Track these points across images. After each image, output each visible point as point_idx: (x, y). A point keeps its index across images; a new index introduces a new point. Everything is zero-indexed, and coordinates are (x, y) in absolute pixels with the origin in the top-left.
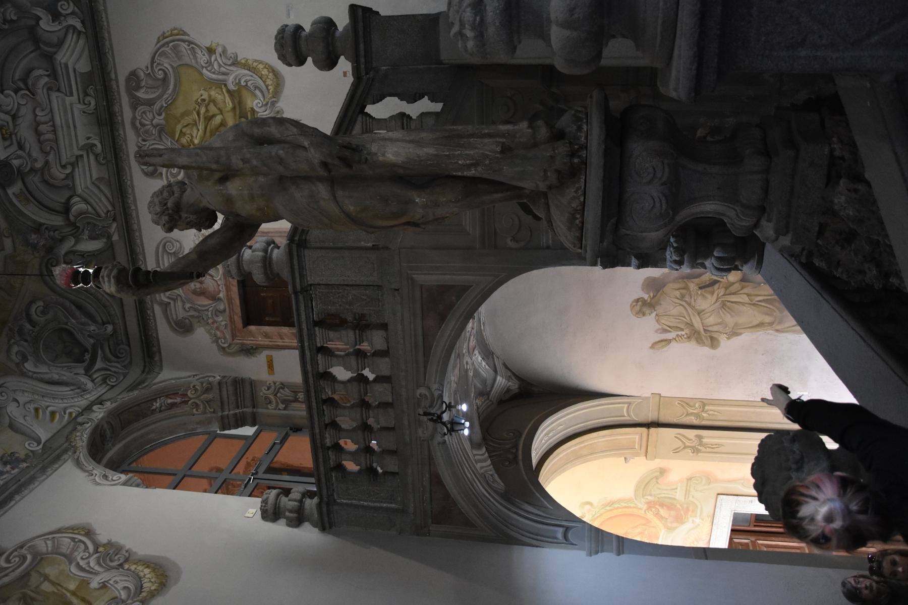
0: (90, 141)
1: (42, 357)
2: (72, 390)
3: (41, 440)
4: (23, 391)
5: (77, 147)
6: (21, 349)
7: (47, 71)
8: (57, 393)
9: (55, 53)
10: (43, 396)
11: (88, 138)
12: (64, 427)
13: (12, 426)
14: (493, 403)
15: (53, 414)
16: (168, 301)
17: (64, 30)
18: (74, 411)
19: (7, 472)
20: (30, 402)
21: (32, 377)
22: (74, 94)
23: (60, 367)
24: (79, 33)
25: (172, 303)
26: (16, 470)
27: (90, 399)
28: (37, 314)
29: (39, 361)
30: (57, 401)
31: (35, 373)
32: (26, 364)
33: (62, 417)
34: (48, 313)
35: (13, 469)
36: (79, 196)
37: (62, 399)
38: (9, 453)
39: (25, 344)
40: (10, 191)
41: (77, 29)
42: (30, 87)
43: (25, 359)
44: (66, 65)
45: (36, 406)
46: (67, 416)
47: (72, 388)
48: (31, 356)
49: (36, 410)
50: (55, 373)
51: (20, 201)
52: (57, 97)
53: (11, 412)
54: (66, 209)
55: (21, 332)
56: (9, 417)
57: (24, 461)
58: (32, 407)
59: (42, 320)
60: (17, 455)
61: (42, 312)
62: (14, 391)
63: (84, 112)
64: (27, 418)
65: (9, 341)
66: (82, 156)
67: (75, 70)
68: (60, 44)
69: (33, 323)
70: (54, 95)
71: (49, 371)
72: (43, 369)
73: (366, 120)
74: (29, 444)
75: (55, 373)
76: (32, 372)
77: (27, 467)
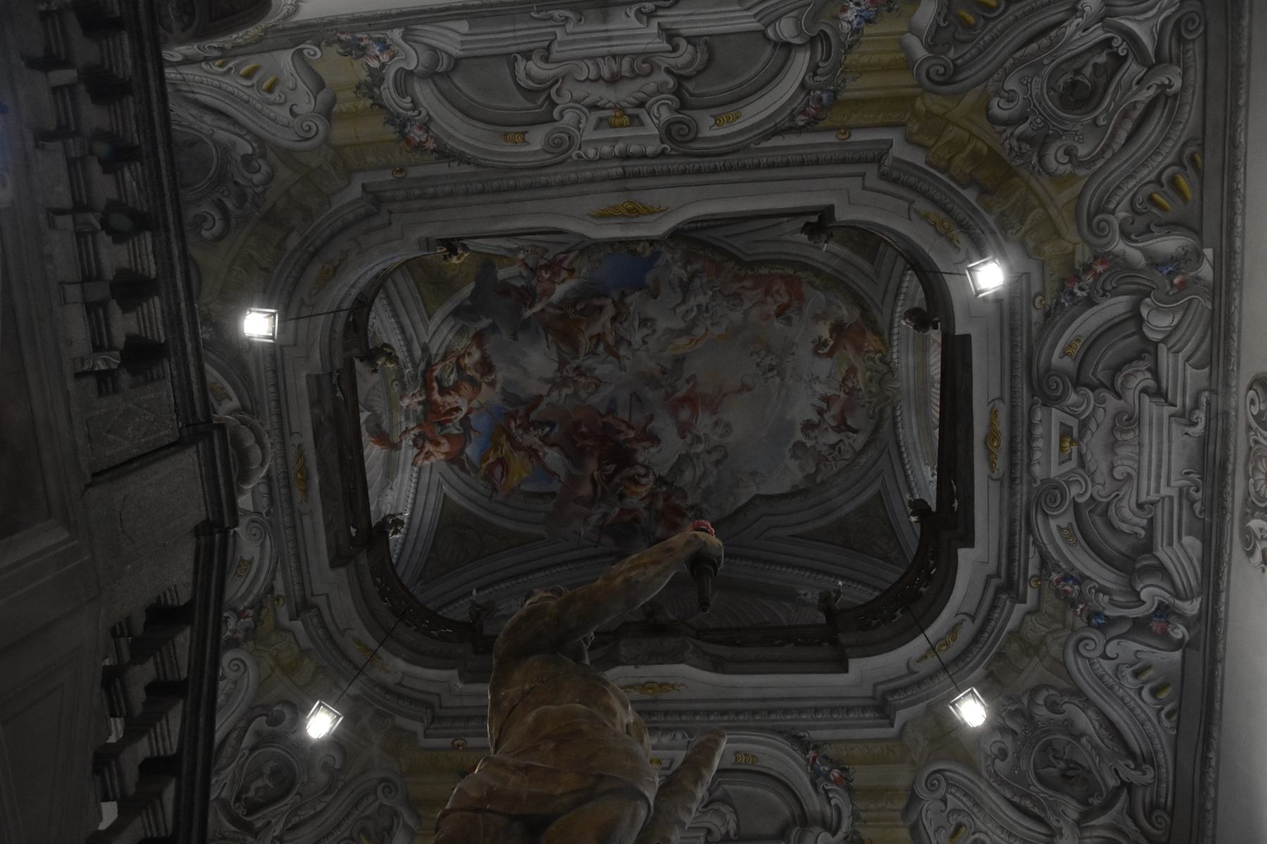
1: (217, 152)
2: (193, 92)
3: (294, 54)
4: (274, 120)
6: (246, 174)
7: (735, 835)
8: (222, 99)
10: (248, 102)
12: (242, 55)
13: (321, 85)
14: (312, 595)
15: (248, 76)
19: (371, 38)
20: (273, 104)
21: (249, 131)
23: (193, 129)
26: (359, 36)
27: (175, 71)
28: (214, 219)
29: (225, 150)
30: (230, 89)
31: (239, 135)
32: (250, 151)
33: (238, 67)
34: (195, 216)
35: (361, 39)
37: (220, 87)
38: (348, 57)
39: (239, 180)
40: (235, 403)
42: (715, 806)
43: (247, 160)
45: (269, 96)
46: (230, 65)
47: (190, 95)
48: (235, 160)
49: (270, 90)
50: (207, 124)
51: (223, 388)
53: (310, 101)
55: (242, 198)
56: (315, 98)
57: (340, 41)
58: (273, 97)
59: (206, 208)
60: (341, 51)
61: (205, 219)
62: (287, 126)
64: (291, 85)
65: (264, 191)
69: (221, 206)
71: (215, 130)
72: (223, 136)
74: (315, 55)
75: (207, 124)
76: (244, 139)
77: (342, 33)
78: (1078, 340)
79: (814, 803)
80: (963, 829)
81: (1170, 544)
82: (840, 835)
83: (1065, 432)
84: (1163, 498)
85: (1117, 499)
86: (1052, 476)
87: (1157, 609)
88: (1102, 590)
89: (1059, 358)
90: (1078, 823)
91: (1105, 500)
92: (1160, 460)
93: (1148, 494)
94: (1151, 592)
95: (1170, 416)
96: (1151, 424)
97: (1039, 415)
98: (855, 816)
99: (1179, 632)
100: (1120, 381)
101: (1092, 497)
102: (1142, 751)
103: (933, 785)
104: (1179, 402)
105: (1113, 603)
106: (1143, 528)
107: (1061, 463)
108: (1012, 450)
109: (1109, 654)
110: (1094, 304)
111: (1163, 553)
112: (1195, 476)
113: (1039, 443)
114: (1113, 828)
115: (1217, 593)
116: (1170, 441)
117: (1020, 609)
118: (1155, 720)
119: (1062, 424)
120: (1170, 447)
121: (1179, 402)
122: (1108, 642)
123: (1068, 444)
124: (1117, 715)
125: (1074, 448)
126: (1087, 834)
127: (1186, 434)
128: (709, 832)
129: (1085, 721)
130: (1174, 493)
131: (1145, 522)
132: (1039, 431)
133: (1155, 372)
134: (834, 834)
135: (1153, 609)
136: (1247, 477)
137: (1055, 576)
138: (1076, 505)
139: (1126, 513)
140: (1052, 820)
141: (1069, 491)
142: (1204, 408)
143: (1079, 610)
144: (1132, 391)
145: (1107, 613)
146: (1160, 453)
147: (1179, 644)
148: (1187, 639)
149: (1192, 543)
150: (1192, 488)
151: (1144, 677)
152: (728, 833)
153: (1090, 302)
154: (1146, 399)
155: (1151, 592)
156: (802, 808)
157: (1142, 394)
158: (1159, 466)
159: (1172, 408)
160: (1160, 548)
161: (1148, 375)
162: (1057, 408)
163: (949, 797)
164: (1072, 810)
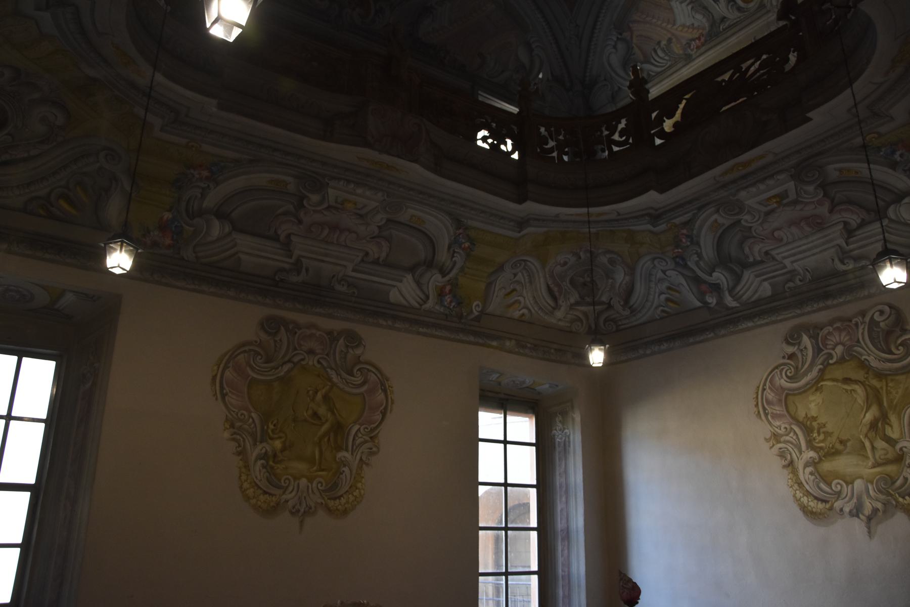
0: (304, 270)
5: (303, 257)
6: (668, 296)
9: (413, 276)
11: (307, 270)
17: (427, 293)
24: (421, 305)
44: (401, 281)
52: (358, 256)
54: (220, 214)
63: (334, 276)
66: (291, 257)
67: (394, 286)
68: (418, 284)
73: (877, 241)
78: (857, 173)
79: (443, 256)
80: (515, 292)
81: (757, 276)
82: (447, 278)
83: (782, 196)
84: (782, 263)
85: (761, 240)
86: (746, 203)
87: (712, 284)
88: (700, 256)
89: (832, 171)
90: (572, 305)
91: (755, 234)
92: (804, 251)
93: (778, 254)
94: (720, 277)
95: (838, 245)
96: (825, 236)
97: (781, 177)
98: (462, 269)
99: (712, 300)
100: (843, 207)
101: (751, 227)
102: (634, 304)
103: (516, 266)
104: (851, 247)
105: (697, 264)
106: (754, 259)
107: (760, 203)
108: (744, 177)
109: (667, 273)
110: (894, 169)
111: (748, 275)
112: (809, 276)
113: (762, 187)
114: (585, 314)
115: (750, 318)
116: (821, 252)
117: (650, 227)
118: (654, 306)
119: (786, 191)
120: (817, 253)
121: (851, 247)
122: (673, 270)
123: (775, 201)
124: (640, 289)
125: (775, 205)
126: (571, 312)
127: (833, 260)
128: (367, 254)
129: (620, 277)
130: (789, 267)
131: (759, 259)
132: (771, 182)
133: (861, 226)
134: (444, 276)
135: (712, 282)
136: (831, 323)
137: (685, 231)
138: (739, 221)
139: (756, 248)
140: (560, 302)
141: (745, 215)
142: (857, 265)
143: (676, 250)
144: (841, 216)
145: (689, 263)
146: (809, 249)
147: (706, 304)
148: (712, 306)
149: (766, 289)
150: (800, 277)
151: (670, 292)
152: (379, 258)
153: (894, 166)
154: (841, 226)
155: (720, 277)
156: (434, 257)
157: (842, 223)
158: (800, 253)
159: (844, 244)
160: (750, 272)
161: (859, 221)
162: (795, 185)
163: (520, 274)
164: (574, 298)
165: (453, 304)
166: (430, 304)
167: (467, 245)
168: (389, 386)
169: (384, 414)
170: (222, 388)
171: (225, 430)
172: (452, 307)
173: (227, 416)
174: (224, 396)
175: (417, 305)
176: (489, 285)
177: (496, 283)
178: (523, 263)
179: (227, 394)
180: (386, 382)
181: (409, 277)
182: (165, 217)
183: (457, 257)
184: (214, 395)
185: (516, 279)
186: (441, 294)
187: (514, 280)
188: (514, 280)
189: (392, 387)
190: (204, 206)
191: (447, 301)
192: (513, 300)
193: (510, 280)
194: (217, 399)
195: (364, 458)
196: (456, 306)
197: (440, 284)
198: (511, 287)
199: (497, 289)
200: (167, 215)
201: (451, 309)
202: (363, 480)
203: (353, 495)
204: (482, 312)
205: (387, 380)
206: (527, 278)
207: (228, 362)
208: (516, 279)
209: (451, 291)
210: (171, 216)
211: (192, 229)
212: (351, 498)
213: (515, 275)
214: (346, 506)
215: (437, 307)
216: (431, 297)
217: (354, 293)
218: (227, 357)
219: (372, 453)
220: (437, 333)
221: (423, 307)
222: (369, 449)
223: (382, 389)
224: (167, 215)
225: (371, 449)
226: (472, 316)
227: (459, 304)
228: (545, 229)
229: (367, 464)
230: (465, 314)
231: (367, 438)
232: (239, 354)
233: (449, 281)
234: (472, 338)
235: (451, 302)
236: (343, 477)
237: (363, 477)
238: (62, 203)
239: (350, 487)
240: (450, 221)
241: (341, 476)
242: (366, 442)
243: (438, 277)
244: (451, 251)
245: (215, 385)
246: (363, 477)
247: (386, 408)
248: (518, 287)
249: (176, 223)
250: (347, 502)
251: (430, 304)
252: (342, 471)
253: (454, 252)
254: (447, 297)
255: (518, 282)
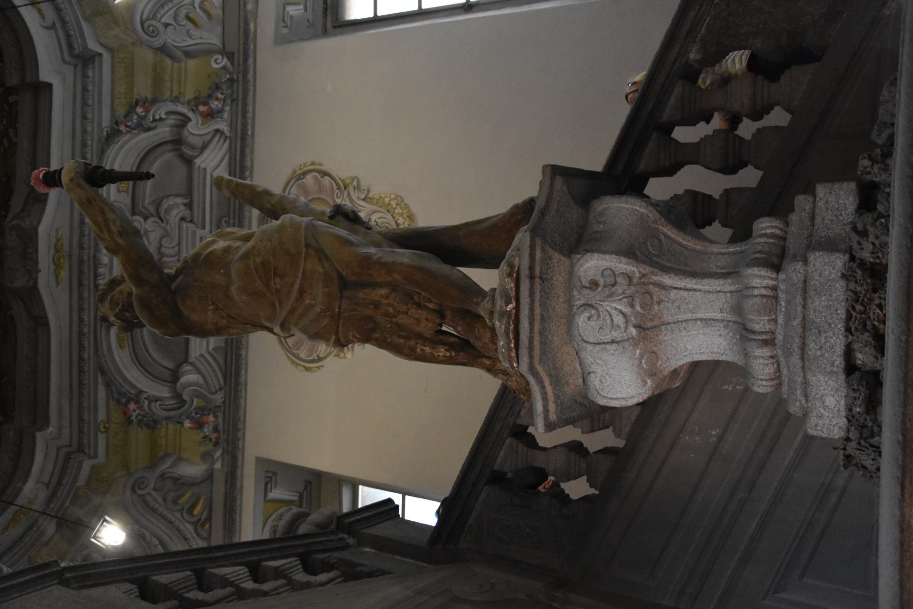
9: (196, 157)
16: (98, 49)
18: (644, 279)
22: (253, 460)
24: (226, 137)
25: (106, 57)
36: (192, 364)
41: (225, 134)
42: (162, 213)
44: (205, 170)
54: (175, 377)
67: (212, 176)
68: (204, 147)
70: (184, 225)
79: (164, 132)
80: (191, 15)
82: (190, 114)
98: (176, 100)
103: (153, 32)
128: (183, 219)
134: (189, 120)
152: (185, 204)
165: (220, 96)
166: (224, 126)
167: (139, 110)
168: (300, 169)
169: (325, 174)
170: (313, 361)
171: (346, 358)
172: (223, 96)
173: (334, 356)
174: (320, 359)
175: (227, 142)
176: (189, 55)
177: (183, 47)
178: (147, 23)
179: (318, 356)
180: (296, 174)
181: (198, 161)
182: (189, 425)
183: (160, 115)
184: (320, 369)
185: (172, 22)
186: (211, 115)
187: (174, 24)
188: (174, 24)
189: (301, 165)
190: (168, 395)
191: (217, 105)
192: (201, 13)
193: (175, 29)
194: (322, 366)
195: (363, 196)
196: (221, 91)
197: (200, 119)
198: (183, 23)
199: (192, 42)
200: (187, 424)
201: (225, 97)
202: (383, 195)
203: (395, 208)
204: (223, 52)
205: (295, 173)
206: (166, 8)
207: (294, 355)
208: (172, 22)
209: (205, 104)
210: (187, 421)
211: (195, 400)
212: (398, 210)
213: (167, 25)
214: (405, 216)
215: (226, 115)
216: (216, 127)
217: (226, 221)
218: (290, 355)
219: (358, 188)
220: (251, 110)
221: (228, 134)
222: (355, 190)
223: (303, 179)
224: (187, 424)
225: (355, 187)
226: (229, 65)
227: (217, 87)
228: (84, 24)
229: (369, 191)
230: (228, 76)
231: (346, 193)
232: (287, 344)
233: (193, 111)
234: (251, 60)
235: (217, 99)
236: (380, 221)
237: (380, 197)
238: (197, 511)
239: (388, 211)
240: (113, 145)
241: (379, 224)
242: (349, 195)
243: (191, 127)
244: (153, 125)
245: (312, 368)
246: (380, 197)
247: (319, 172)
248: (183, 13)
249: (193, 415)
250: (402, 215)
251: (224, 126)
252: (375, 224)
253: (154, 120)
254: (213, 106)
255: (176, 17)
